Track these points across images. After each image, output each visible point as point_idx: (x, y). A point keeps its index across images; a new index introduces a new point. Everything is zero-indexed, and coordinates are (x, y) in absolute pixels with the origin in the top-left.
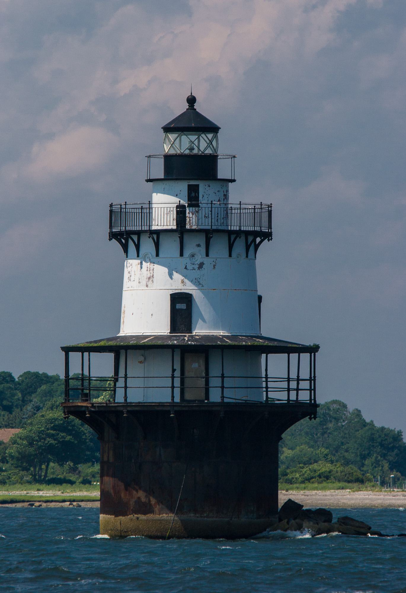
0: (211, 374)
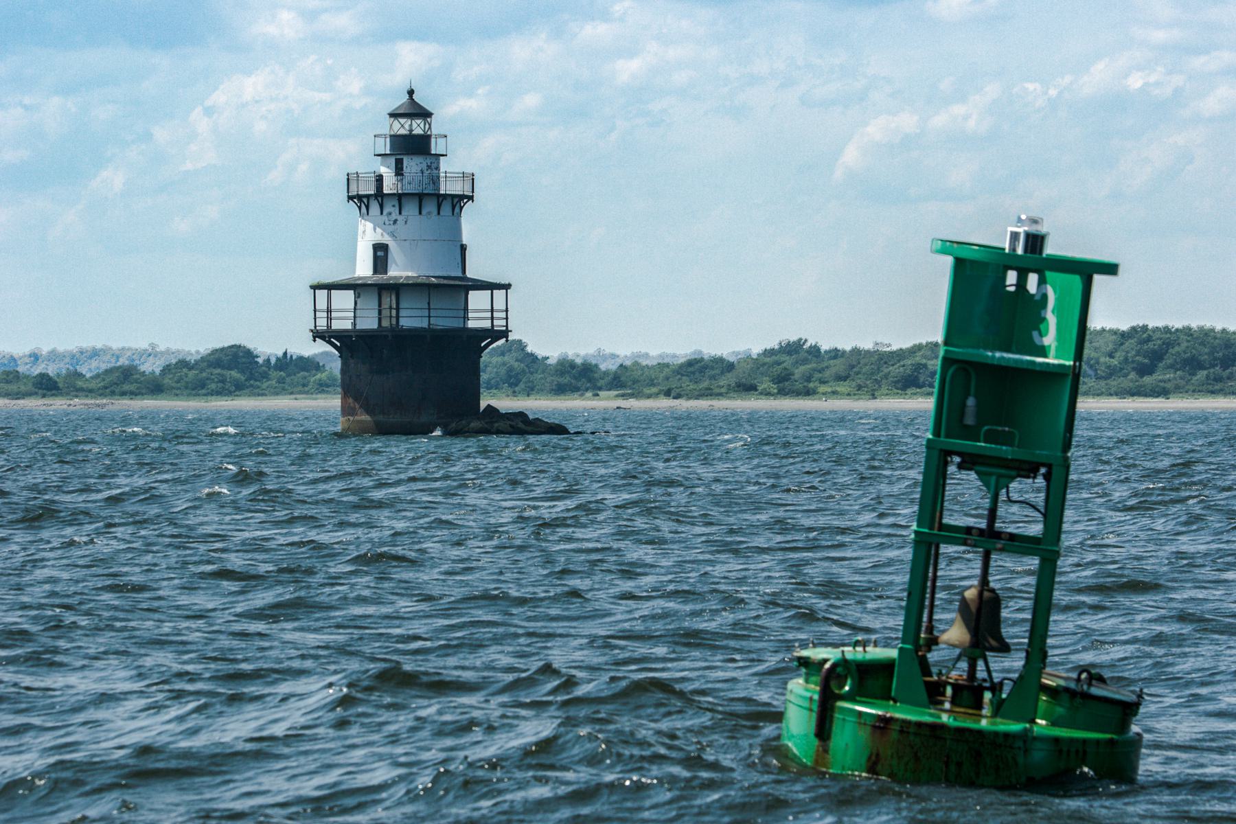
0: (401, 306)
